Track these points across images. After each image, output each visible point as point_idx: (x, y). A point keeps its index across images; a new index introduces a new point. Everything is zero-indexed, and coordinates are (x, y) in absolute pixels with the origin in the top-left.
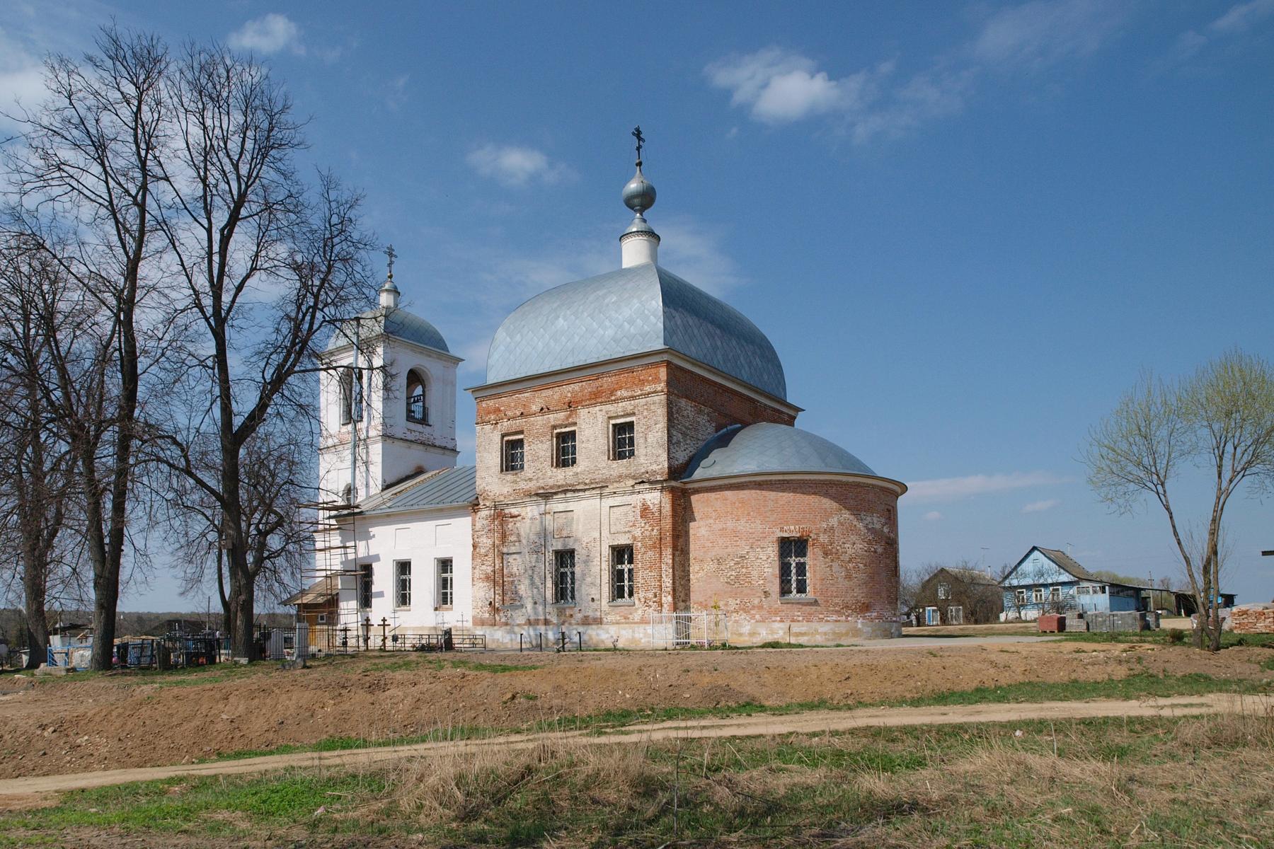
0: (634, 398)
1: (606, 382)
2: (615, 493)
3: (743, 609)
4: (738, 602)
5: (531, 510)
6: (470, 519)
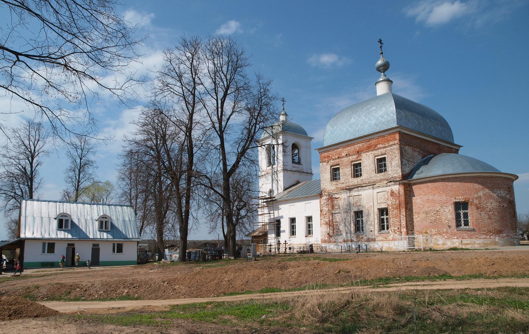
0: (385, 147)
1: (373, 142)
2: (379, 187)
4: (436, 230)
5: (343, 196)
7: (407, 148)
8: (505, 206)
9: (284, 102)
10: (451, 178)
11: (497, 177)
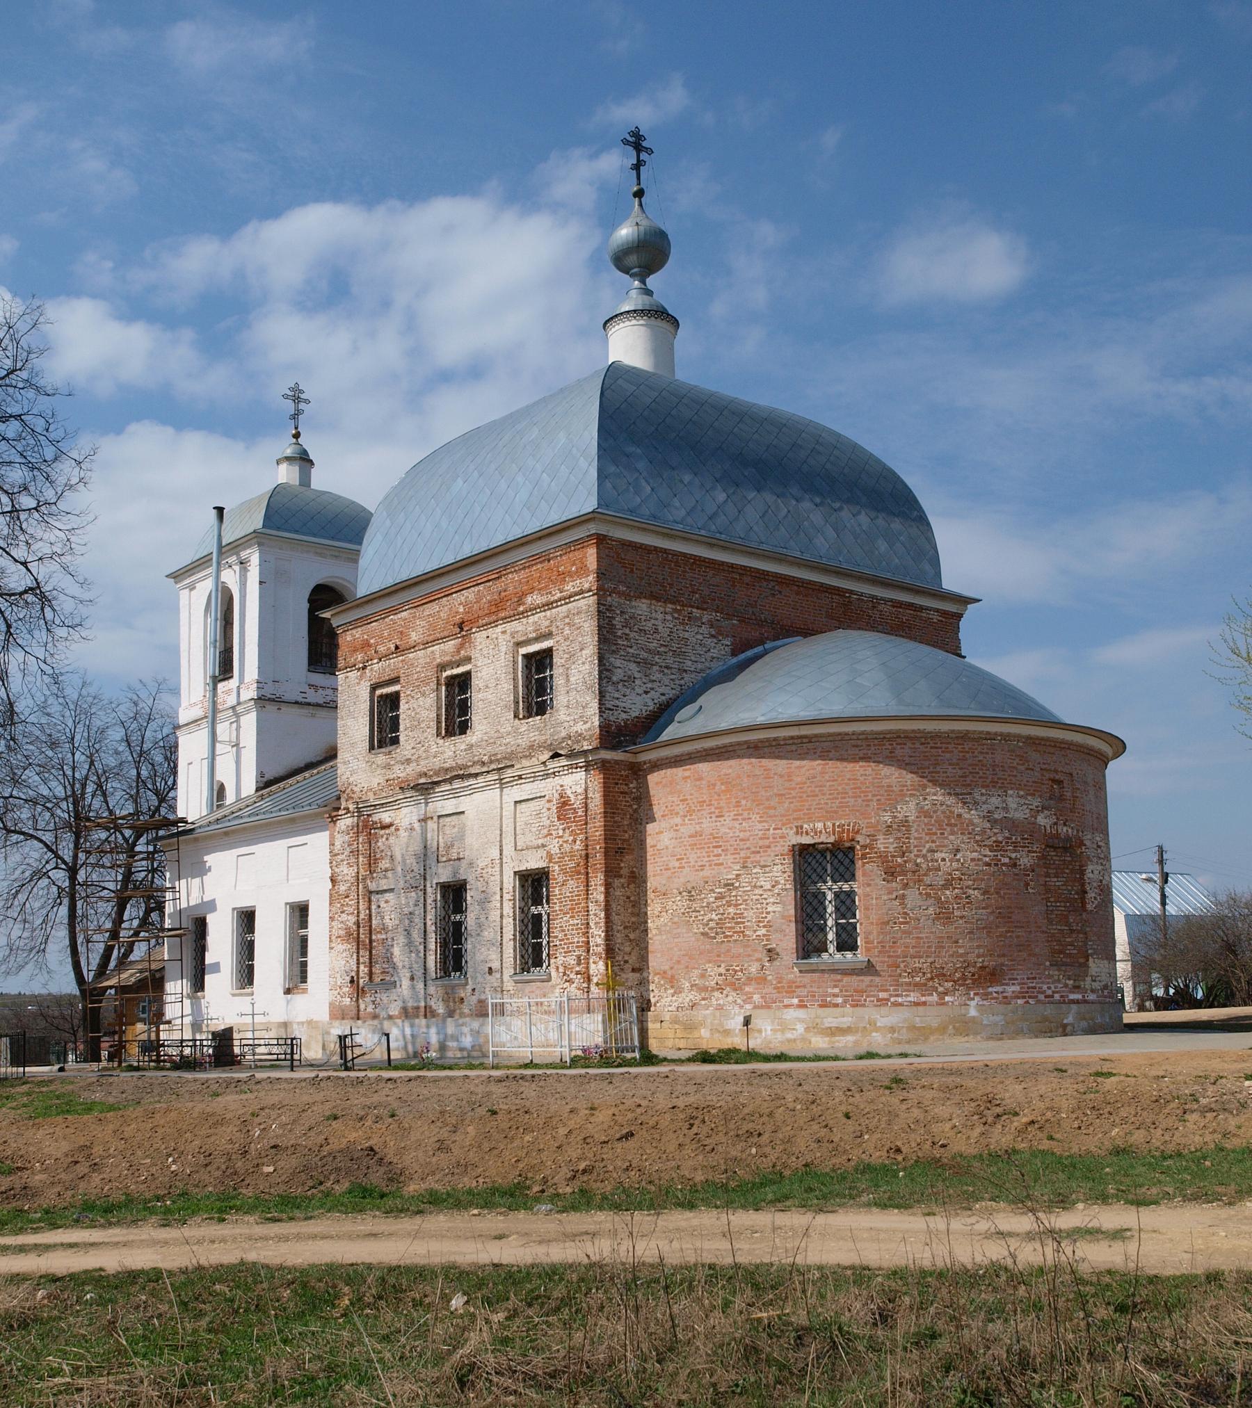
0: (549, 605)
1: (512, 581)
2: (520, 777)
3: (732, 984)
4: (722, 970)
5: (406, 815)
6: (327, 833)
7: (644, 607)
8: (1025, 860)
9: (302, 406)
10: (785, 739)
11: (990, 736)
